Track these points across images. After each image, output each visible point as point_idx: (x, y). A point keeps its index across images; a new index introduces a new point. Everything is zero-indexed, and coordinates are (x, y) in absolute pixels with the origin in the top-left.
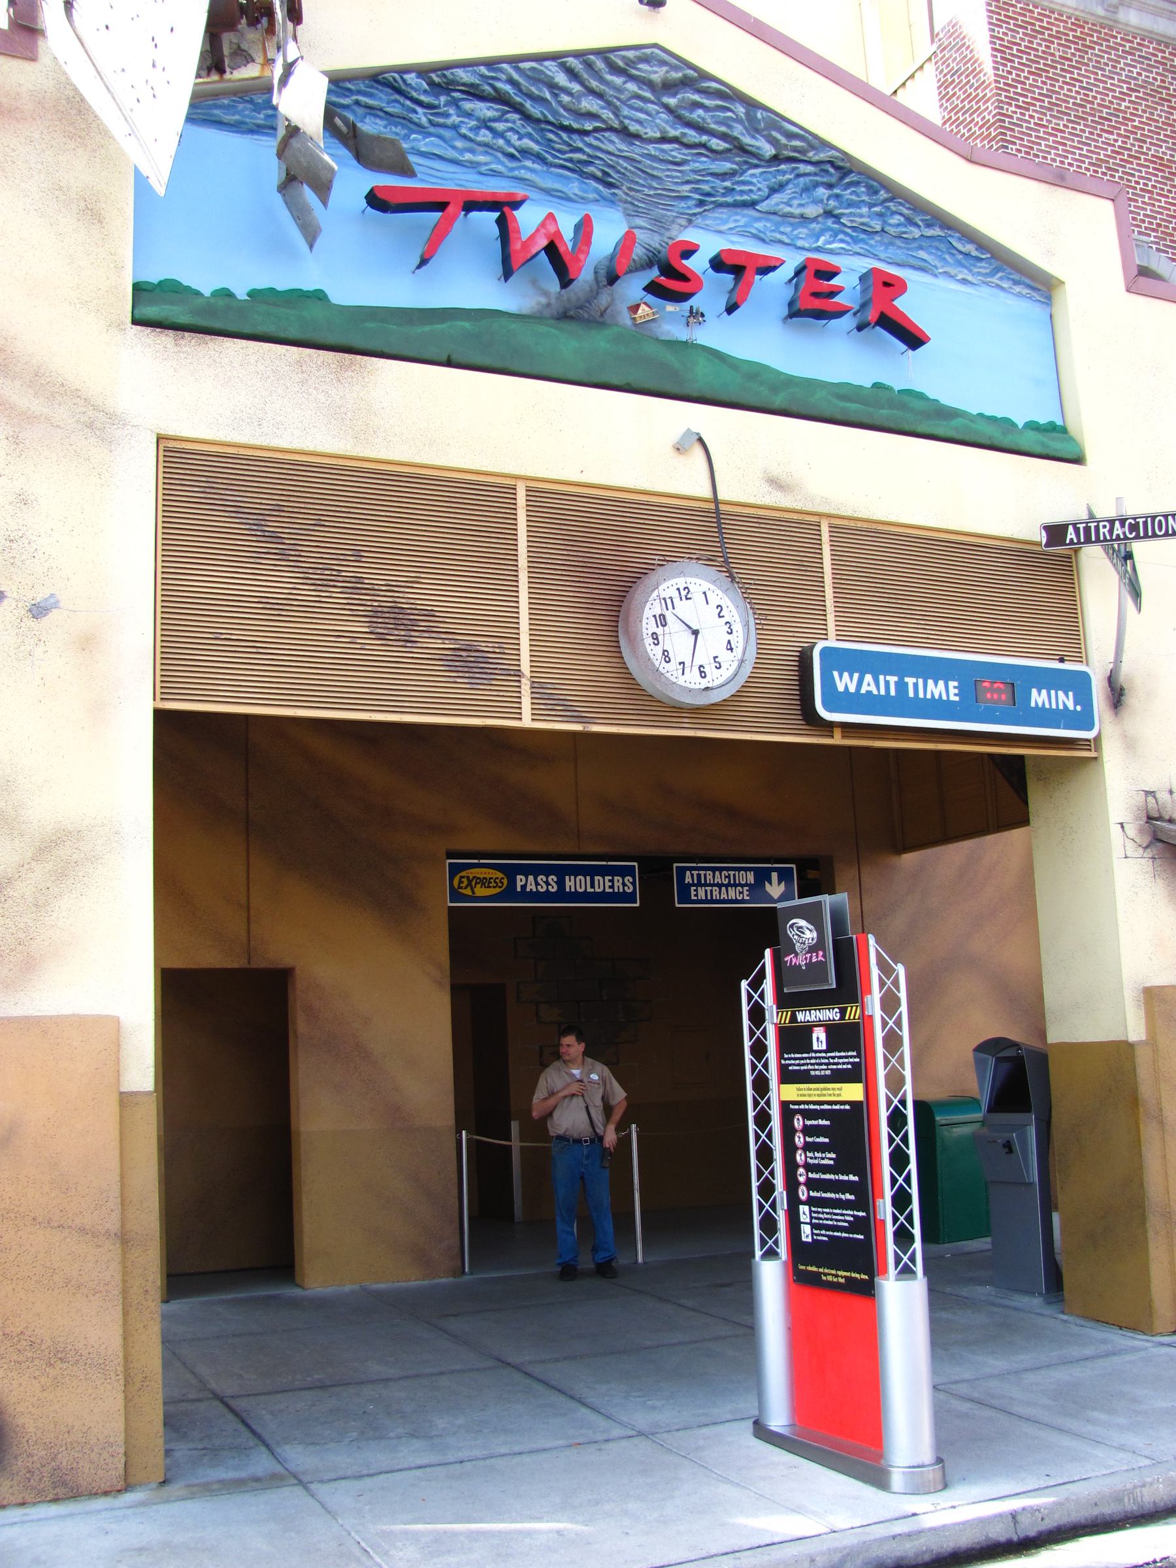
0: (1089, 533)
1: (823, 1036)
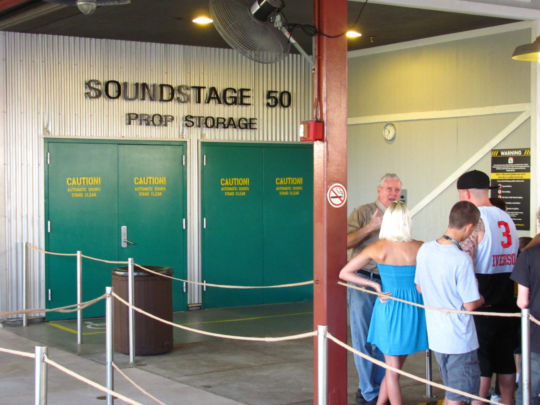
0: (360, 228)
1: (512, 160)
